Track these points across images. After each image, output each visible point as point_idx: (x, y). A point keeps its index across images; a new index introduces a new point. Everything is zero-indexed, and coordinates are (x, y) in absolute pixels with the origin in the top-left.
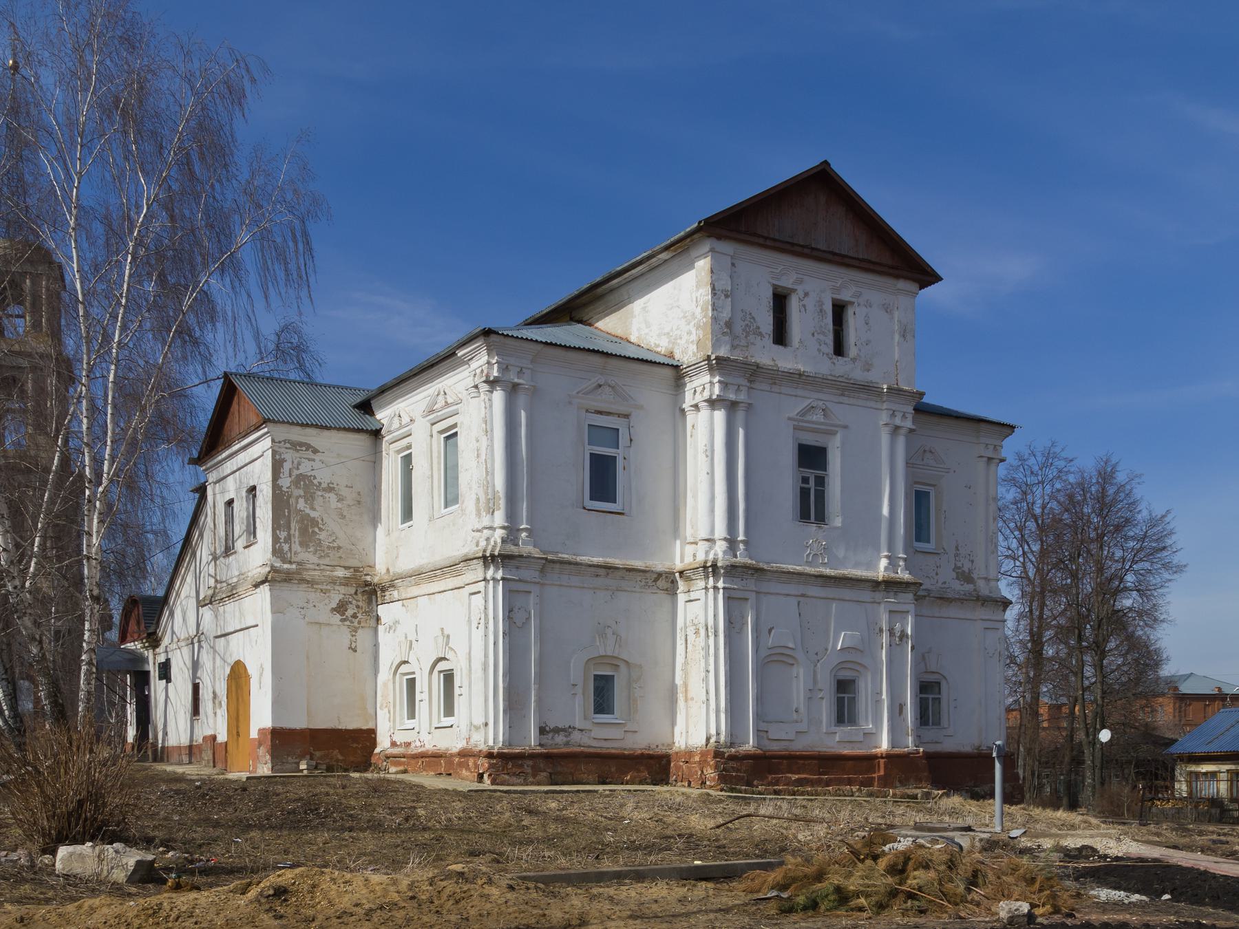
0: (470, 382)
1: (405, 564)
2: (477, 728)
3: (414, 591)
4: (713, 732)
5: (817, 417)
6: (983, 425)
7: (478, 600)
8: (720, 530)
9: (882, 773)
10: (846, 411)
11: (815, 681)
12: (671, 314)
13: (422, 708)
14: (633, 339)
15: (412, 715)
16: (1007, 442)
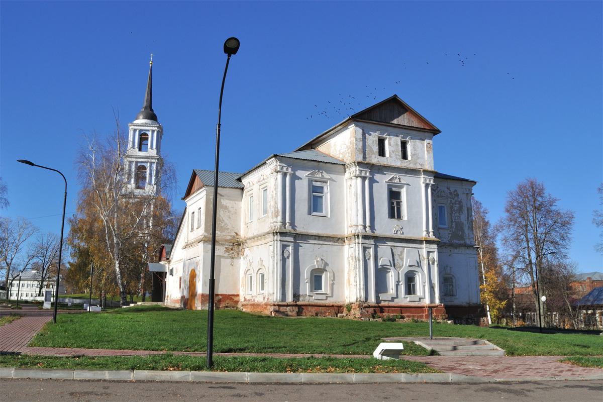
0: (270, 172)
1: (250, 235)
2: (271, 295)
3: (253, 244)
4: (359, 297)
5: (397, 181)
6: (463, 182)
7: (271, 248)
8: (361, 222)
9: (427, 313)
10: (405, 179)
11: (399, 278)
12: (343, 144)
13: (254, 287)
14: (331, 155)
15: (251, 290)
16: (474, 188)
